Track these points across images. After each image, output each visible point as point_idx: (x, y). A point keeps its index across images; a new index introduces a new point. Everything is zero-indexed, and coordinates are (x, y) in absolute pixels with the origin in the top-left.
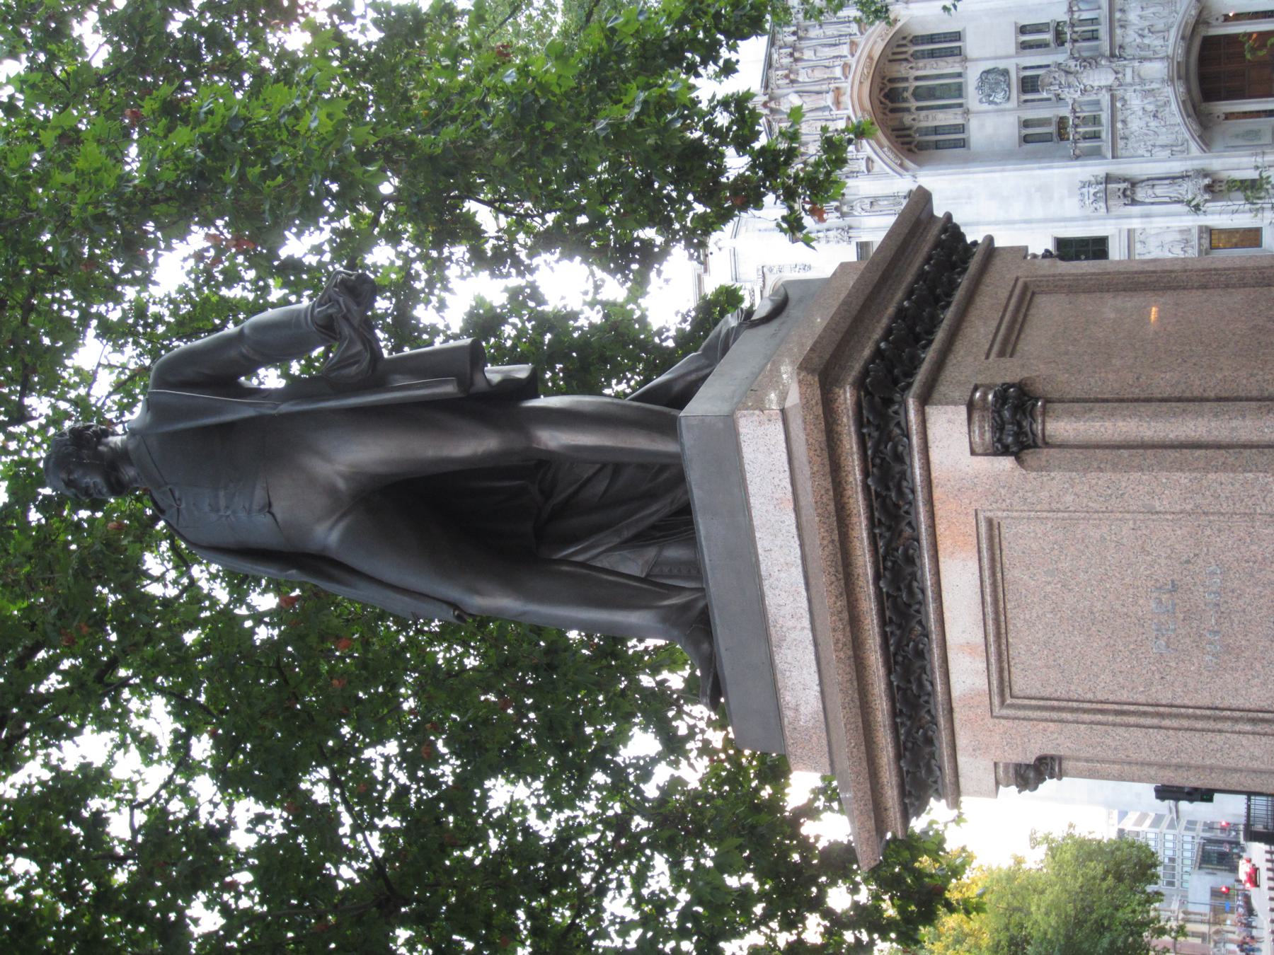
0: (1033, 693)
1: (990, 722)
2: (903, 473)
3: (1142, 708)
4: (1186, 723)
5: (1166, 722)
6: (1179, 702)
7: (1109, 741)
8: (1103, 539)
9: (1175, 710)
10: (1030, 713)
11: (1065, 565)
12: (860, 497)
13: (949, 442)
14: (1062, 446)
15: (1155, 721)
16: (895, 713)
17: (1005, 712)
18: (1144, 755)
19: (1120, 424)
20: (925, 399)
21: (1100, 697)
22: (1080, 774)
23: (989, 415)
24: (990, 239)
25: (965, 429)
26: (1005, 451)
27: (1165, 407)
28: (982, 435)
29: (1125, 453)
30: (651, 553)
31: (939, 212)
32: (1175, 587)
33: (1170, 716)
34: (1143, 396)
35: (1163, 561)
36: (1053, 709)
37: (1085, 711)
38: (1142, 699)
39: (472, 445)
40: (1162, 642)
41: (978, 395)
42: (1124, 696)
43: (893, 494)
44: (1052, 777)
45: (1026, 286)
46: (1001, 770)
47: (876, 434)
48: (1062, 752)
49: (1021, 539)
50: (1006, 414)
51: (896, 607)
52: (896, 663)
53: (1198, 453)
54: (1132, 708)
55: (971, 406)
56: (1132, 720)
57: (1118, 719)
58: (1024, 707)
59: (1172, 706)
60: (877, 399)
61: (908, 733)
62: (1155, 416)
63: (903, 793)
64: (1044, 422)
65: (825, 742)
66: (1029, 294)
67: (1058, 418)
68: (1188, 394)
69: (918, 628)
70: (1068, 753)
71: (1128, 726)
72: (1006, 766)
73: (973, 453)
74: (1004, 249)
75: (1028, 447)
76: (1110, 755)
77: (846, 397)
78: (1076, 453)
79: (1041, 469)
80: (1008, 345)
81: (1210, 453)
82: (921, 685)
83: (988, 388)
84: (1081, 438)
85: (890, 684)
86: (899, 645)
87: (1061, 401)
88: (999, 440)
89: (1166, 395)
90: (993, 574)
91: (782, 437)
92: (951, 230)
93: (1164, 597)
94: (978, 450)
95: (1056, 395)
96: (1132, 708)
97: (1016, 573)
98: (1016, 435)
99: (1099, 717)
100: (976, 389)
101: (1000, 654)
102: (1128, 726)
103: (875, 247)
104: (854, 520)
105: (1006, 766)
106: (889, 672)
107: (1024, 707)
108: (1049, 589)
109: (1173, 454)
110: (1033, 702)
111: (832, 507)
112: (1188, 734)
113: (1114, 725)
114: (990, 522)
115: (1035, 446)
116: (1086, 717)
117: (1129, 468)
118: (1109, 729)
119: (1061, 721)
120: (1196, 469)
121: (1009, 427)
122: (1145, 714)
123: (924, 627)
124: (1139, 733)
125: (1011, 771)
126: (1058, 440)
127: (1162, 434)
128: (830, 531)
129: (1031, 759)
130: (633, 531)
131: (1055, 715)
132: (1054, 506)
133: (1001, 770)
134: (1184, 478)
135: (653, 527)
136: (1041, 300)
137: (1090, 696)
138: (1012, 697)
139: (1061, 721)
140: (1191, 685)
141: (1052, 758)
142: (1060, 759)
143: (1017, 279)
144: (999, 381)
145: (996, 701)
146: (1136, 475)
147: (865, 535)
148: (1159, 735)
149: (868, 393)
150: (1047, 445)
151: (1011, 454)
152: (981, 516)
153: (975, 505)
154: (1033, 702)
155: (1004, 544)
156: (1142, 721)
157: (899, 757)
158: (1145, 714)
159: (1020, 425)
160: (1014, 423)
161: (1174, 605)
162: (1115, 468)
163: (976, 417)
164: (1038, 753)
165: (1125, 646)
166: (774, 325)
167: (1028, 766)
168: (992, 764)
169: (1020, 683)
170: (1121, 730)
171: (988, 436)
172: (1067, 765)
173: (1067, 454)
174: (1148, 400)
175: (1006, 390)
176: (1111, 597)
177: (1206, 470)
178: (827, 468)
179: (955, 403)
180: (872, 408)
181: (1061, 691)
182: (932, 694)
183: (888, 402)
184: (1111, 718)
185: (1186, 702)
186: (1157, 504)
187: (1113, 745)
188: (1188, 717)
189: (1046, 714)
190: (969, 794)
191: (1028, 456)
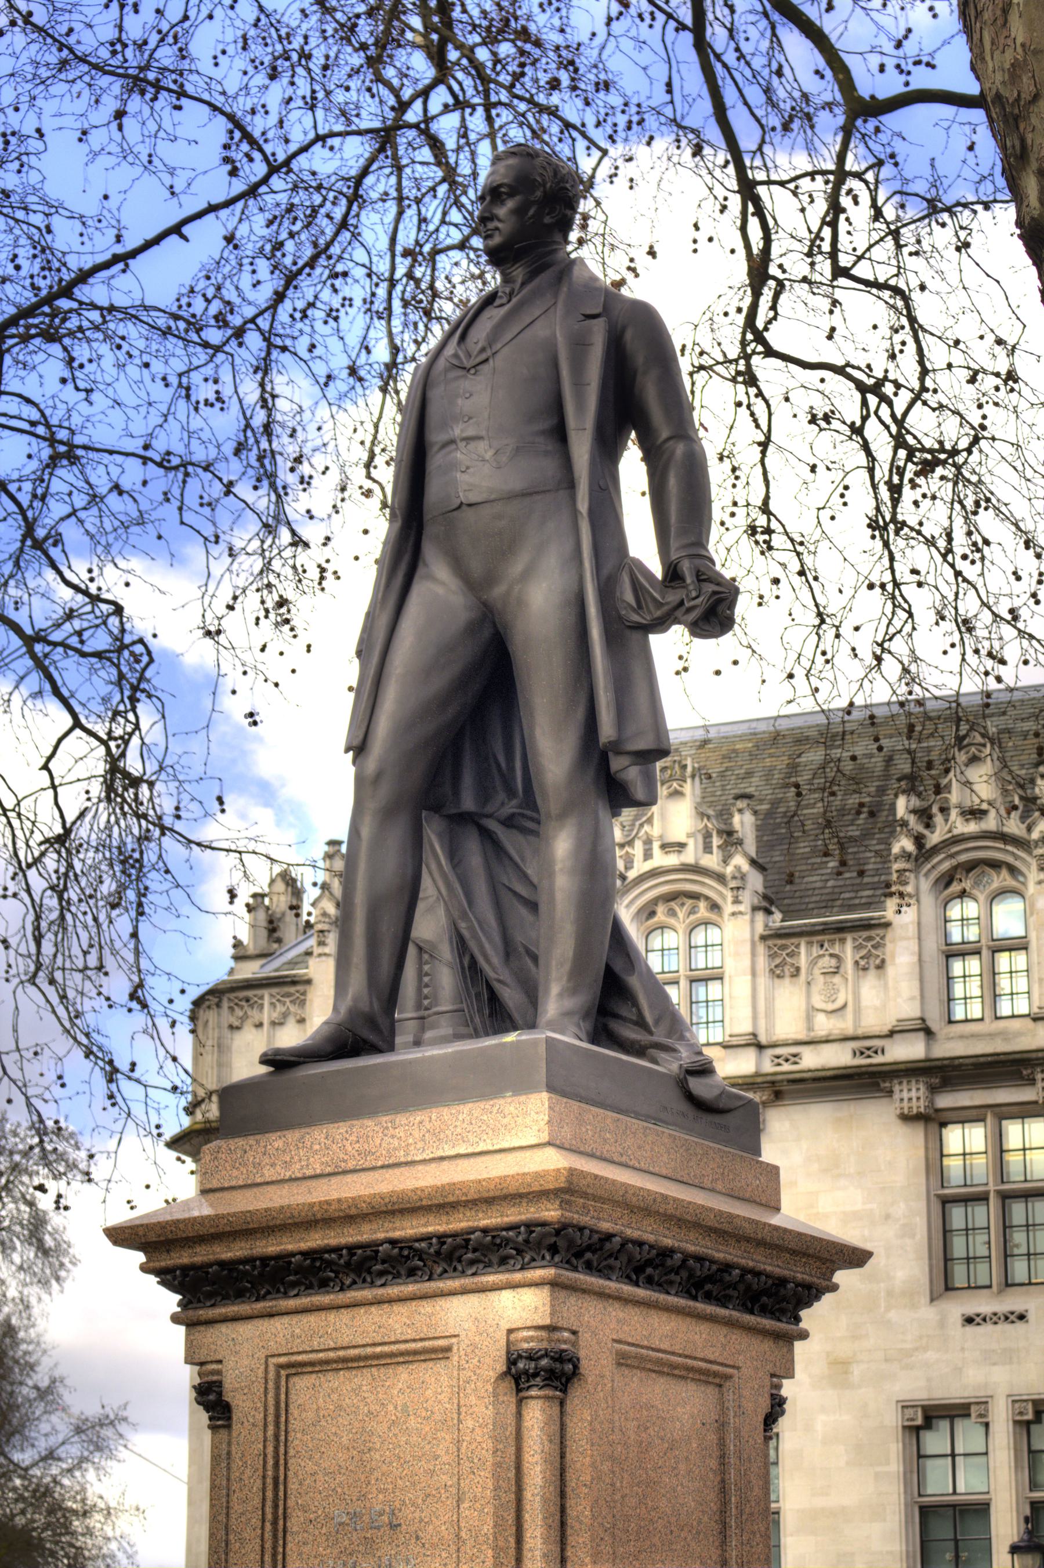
0: (293, 1397)
1: (261, 1354)
2: (489, 1265)
3: (281, 1503)
4: (268, 1545)
5: (268, 1527)
6: (289, 1538)
7: (248, 1472)
8: (436, 1457)
9: (280, 1534)
10: (271, 1395)
11: (412, 1422)
12: (464, 1225)
13: (515, 1307)
14: (519, 1415)
15: (269, 1516)
16: (265, 1260)
17: (272, 1369)
18: (237, 1507)
19: (538, 1468)
20: (554, 1284)
21: (291, 1461)
22: (214, 1447)
23: (545, 1345)
24: (804, 1335)
25: (529, 1324)
26: (511, 1362)
27: (555, 1509)
28: (527, 1340)
29: (512, 1474)
30: (446, 952)
31: (840, 1277)
32: (394, 1527)
33: (275, 1531)
34: (568, 1490)
35: (417, 1515)
36: (277, 1416)
37: (276, 1448)
38: (291, 1503)
39: (552, 751)
40: (345, 1519)
41: (566, 1334)
42: (293, 1486)
43: (470, 1255)
44: (211, 1419)
45: (728, 1377)
46: (214, 1366)
47: (520, 1239)
48: (236, 1427)
49: (434, 1382)
50: (544, 1362)
51: (366, 1259)
52: (314, 1260)
53: (512, 1540)
54: (281, 1494)
55: (551, 1328)
56: (269, 1494)
57: (269, 1481)
58: (277, 1388)
59: (285, 1531)
60: (553, 1239)
61: (246, 1273)
62: (545, 1500)
63: (185, 1269)
64: (538, 1397)
65: (233, 1183)
66: (717, 1381)
67: (543, 1410)
68: (569, 1531)
69: (348, 1282)
70: (234, 1434)
71: (264, 1490)
72: (219, 1372)
73: (510, 1331)
74: (791, 1351)
75: (517, 1384)
76: (235, 1475)
77: (551, 1213)
78: (511, 1429)
79: (495, 1395)
80: (628, 1360)
81: (512, 1552)
82: (294, 1285)
83: (574, 1344)
84: (525, 1433)
85: (293, 1254)
86: (330, 1263)
87: (562, 1413)
88: (520, 1356)
89: (568, 1511)
90: (402, 1354)
91: (524, 1143)
92: (810, 1293)
93: (385, 1518)
94: (513, 1336)
95: (569, 1408)
96: (281, 1494)
97: (404, 1376)
98: (526, 1372)
99: (271, 1462)
100: (574, 1333)
101: (327, 1362)
102: (264, 1490)
103: (775, 1220)
104: (444, 1218)
105: (219, 1372)
106: (305, 1254)
107: (277, 1388)
108: (391, 1407)
109: (511, 1518)
110: (283, 1397)
111: (451, 1199)
112: (258, 1548)
113: (264, 1477)
114: (448, 1349)
115: (519, 1390)
116: (270, 1449)
117: (496, 1477)
118: (260, 1472)
119: (265, 1425)
120: (496, 1538)
121: (533, 1365)
122: (276, 1506)
123: (349, 1287)
124: (257, 1501)
125: (215, 1378)
126: (524, 1413)
127: (577, 1526)
128: (430, 1197)
129: (228, 1397)
130: (466, 934)
131: (271, 1418)
132: (463, 1409)
133: (214, 1366)
134: (488, 1528)
135: (473, 962)
136: (711, 1391)
137: (291, 1452)
138: (288, 1376)
139: (265, 1425)
140: (306, 1549)
141: (230, 1418)
142: (228, 1427)
143: (738, 1368)
144: (582, 1354)
145: (282, 1360)
146: (490, 1485)
147: (430, 1229)
148: (256, 1521)
149: (558, 1232)
150: (520, 1402)
151: (509, 1369)
152: (454, 1340)
153: (463, 1334)
154: (283, 1397)
155: (430, 1364)
156: (269, 1503)
157: (222, 1264)
158: (276, 1506)
159: (535, 1375)
160: (543, 1370)
161: (378, 1528)
162: (498, 1465)
163: (543, 1334)
164: (233, 1404)
165: (340, 1484)
166: (684, 1106)
167: (220, 1394)
168: (970, 1329)
169: (301, 1384)
170: (259, 1483)
171: (526, 1346)
172: (223, 1434)
173: (511, 1420)
174: (563, 1495)
175: (570, 1360)
176: (384, 1468)
177: (495, 1548)
178: (485, 1195)
179: (552, 1314)
180: (544, 1236)
181: (294, 1424)
182: (286, 1295)
183: (554, 1249)
184: (270, 1473)
185: (289, 1546)
186: (466, 1505)
187: (245, 1477)
188: (275, 1548)
189: (271, 1410)
190: (187, 1335)
191: (509, 1384)
